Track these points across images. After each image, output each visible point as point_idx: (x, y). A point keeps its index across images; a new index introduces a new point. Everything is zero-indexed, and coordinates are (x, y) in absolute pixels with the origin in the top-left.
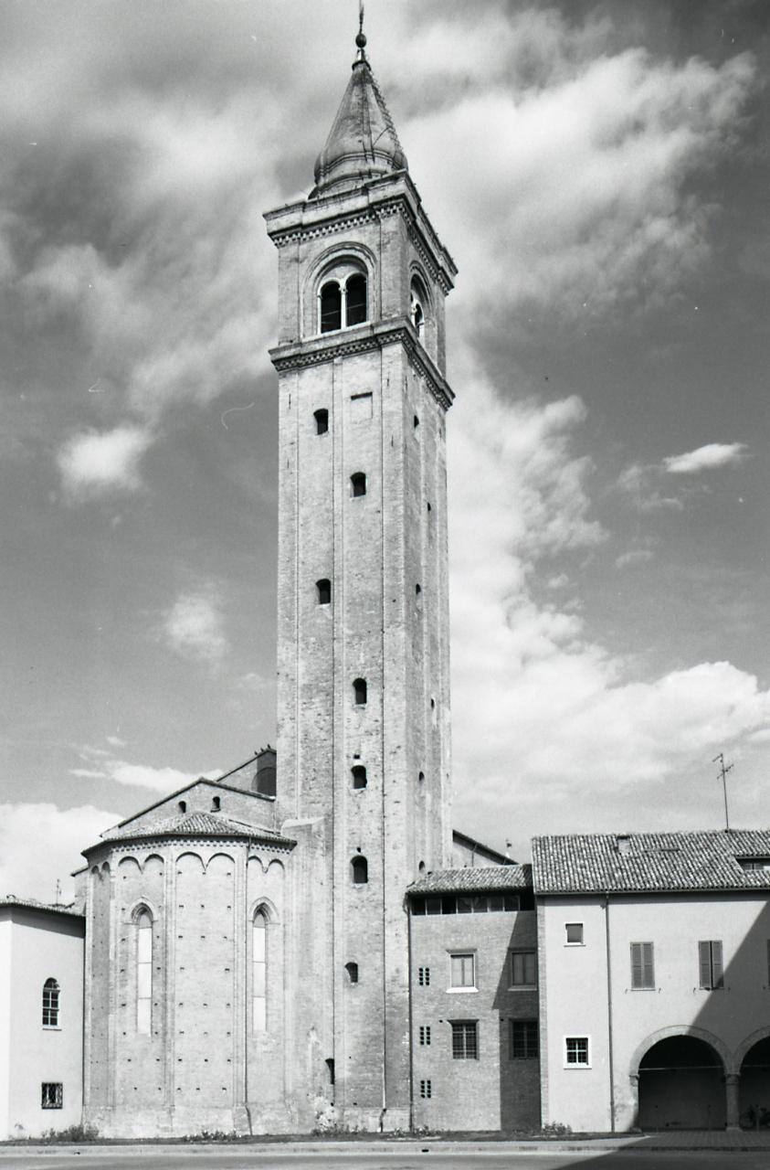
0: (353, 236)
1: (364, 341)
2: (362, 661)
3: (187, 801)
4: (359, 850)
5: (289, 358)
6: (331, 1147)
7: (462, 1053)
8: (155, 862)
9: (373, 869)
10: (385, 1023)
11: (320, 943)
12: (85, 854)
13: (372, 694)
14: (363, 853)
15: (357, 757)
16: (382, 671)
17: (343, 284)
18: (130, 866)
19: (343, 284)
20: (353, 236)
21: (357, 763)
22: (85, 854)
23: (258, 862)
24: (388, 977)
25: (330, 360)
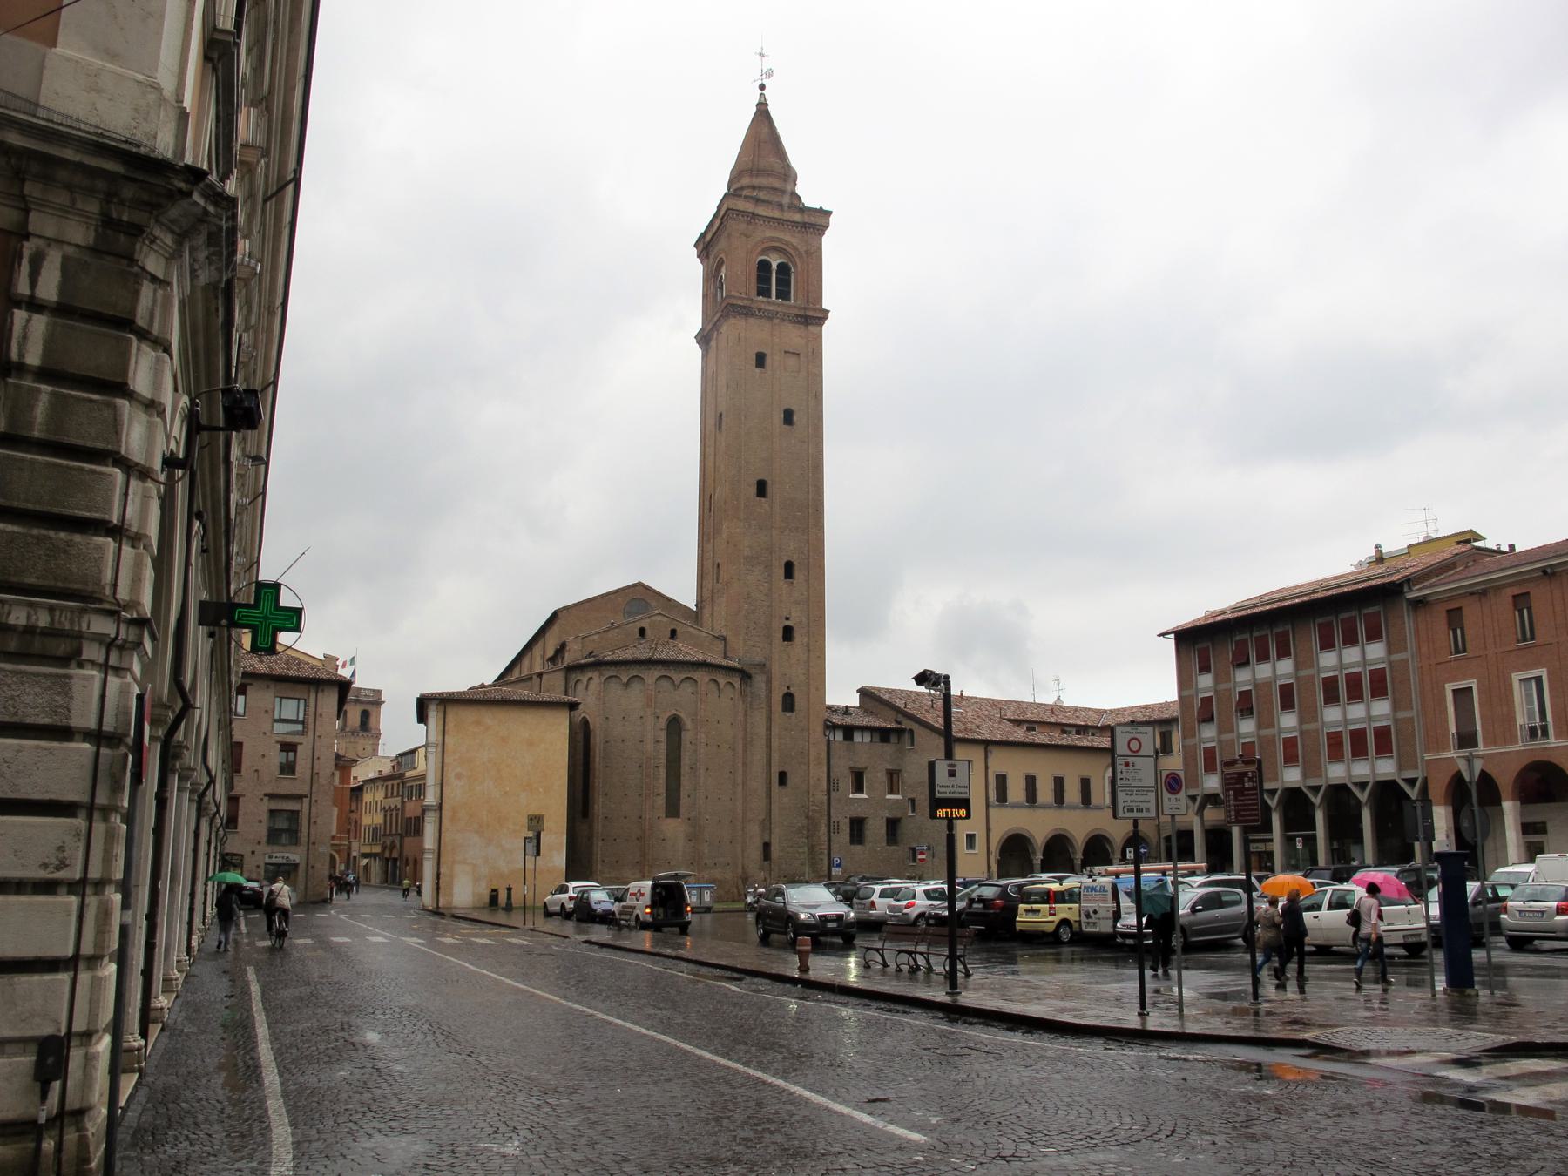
0: (788, 237)
1: (797, 316)
2: (792, 548)
3: (647, 627)
4: (788, 688)
5: (741, 307)
6: (1558, 947)
7: (1333, 864)
8: (687, 685)
9: (799, 702)
10: (807, 817)
11: (758, 757)
12: (864, 693)
13: (798, 574)
14: (792, 690)
15: (787, 619)
16: (808, 559)
17: (774, 266)
18: (665, 684)
19: (774, 266)
20: (788, 237)
21: (787, 623)
22: (864, 693)
23: (618, 680)
24: (812, 782)
25: (771, 319)
